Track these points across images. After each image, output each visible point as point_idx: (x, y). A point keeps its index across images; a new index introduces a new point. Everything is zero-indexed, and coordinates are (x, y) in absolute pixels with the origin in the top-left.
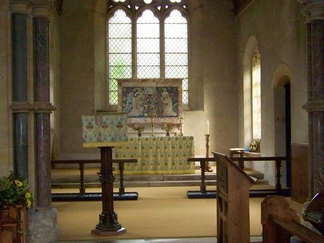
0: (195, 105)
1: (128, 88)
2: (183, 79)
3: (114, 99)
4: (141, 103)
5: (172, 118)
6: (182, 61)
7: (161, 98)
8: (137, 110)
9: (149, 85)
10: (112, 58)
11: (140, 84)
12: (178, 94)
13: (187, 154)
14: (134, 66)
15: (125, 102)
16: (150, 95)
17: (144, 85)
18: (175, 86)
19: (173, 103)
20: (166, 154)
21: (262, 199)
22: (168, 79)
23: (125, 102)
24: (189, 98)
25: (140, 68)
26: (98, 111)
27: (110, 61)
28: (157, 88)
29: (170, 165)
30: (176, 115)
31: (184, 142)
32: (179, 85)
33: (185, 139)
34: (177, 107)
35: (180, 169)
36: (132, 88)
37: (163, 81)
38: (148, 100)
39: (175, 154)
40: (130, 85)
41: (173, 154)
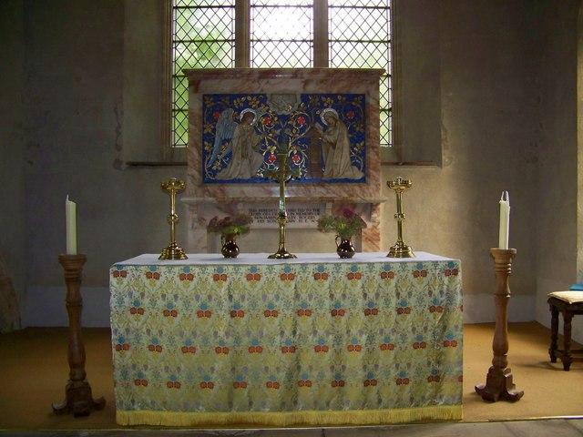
0: (414, 151)
1: (217, 97)
2: (380, 72)
3: (181, 136)
4: (257, 139)
5: (349, 187)
6: (376, 27)
7: (317, 125)
8: (246, 162)
9: (282, 87)
10: (181, 21)
11: (255, 86)
12: (366, 117)
13: (428, 338)
14: (242, 40)
15: (209, 138)
16: (285, 118)
17: (266, 87)
18: (358, 92)
19: (353, 142)
20: (338, 339)
21: (323, 179)
22: (337, 71)
23: (209, 138)
24: (396, 130)
25: (258, 46)
26: (134, 165)
27: (176, 28)
28: (305, 97)
29: (354, 390)
30: (359, 175)
31: (420, 286)
32: (372, 88)
33: (425, 274)
34: (363, 154)
35: (399, 404)
36: (233, 97)
37: (321, 76)
38: (278, 132)
39: (379, 340)
40: (225, 87)
41: (371, 339)
